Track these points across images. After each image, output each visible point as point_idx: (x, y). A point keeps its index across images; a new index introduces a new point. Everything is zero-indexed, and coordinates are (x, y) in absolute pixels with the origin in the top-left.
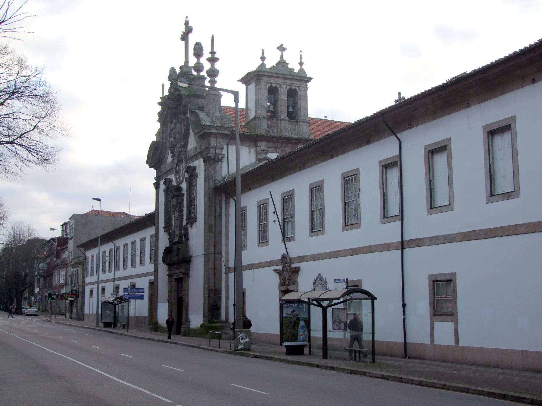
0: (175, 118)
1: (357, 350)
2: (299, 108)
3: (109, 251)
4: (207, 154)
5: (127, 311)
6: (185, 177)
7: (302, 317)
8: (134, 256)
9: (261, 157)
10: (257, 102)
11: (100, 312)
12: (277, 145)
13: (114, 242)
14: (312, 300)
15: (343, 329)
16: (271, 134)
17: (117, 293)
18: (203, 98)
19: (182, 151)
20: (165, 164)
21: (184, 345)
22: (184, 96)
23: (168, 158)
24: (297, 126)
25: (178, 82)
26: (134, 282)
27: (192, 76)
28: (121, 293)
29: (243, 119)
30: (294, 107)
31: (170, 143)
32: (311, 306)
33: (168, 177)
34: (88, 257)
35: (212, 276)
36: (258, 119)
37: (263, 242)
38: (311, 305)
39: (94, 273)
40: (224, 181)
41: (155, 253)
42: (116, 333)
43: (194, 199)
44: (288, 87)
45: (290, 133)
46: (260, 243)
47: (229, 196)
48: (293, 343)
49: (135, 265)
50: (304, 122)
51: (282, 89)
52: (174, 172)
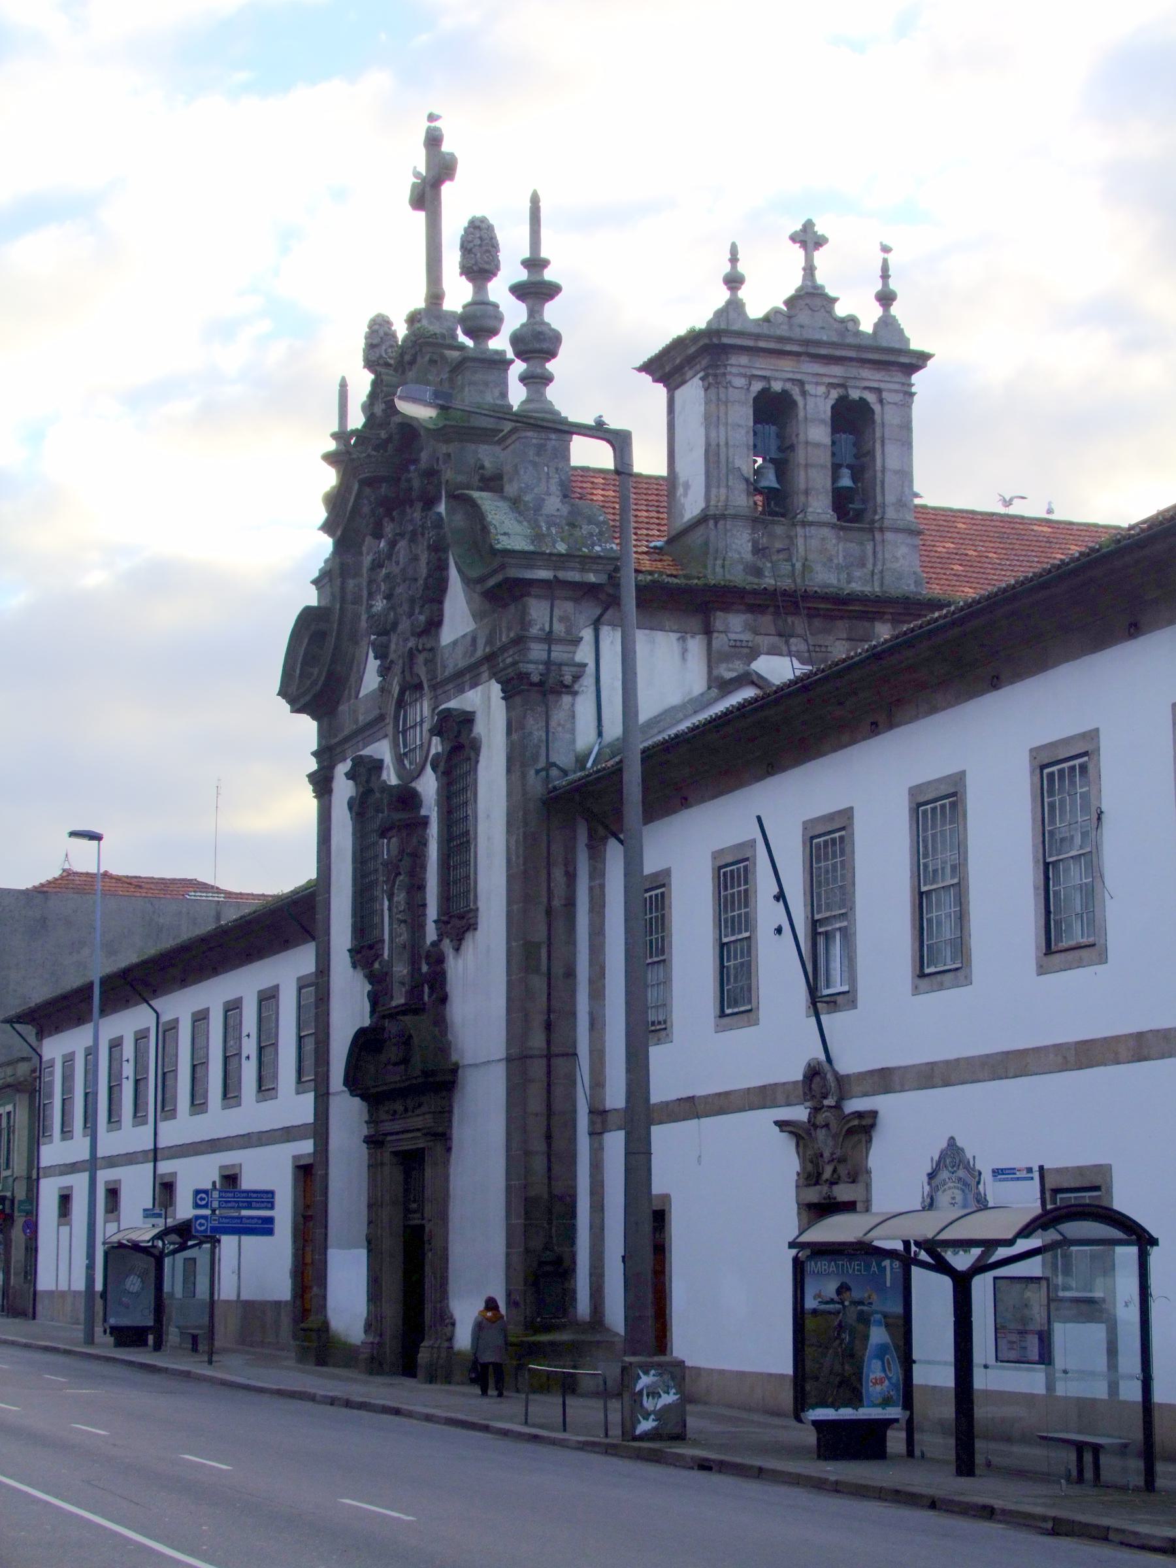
0: (393, 520)
1: (1086, 1443)
2: (879, 475)
3: (136, 1040)
4: (514, 664)
5: (207, 1281)
6: (433, 751)
7: (877, 1312)
8: (233, 1063)
9: (727, 672)
10: (712, 455)
11: (99, 1286)
12: (793, 623)
13: (152, 1003)
14: (917, 1244)
15: (1037, 1358)
16: (768, 581)
17: (170, 1209)
18: (499, 442)
19: (418, 650)
20: (352, 701)
21: (428, 1418)
22: (422, 432)
23: (364, 673)
24: (869, 548)
25: (396, 401)
26: (233, 1166)
27: (455, 354)
28: (184, 1209)
30: (855, 478)
31: (371, 617)
32: (914, 1269)
33: (364, 752)
34: (52, 1061)
35: (539, 1145)
37: (736, 1010)
38: (913, 1267)
39: (76, 1124)
40: (583, 768)
41: (316, 1050)
43: (468, 842)
44: (835, 394)
45: (844, 576)
46: (722, 1015)
47: (601, 831)
48: (846, 1413)
49: (238, 1097)
50: (897, 530)
51: (811, 401)
52: (390, 729)
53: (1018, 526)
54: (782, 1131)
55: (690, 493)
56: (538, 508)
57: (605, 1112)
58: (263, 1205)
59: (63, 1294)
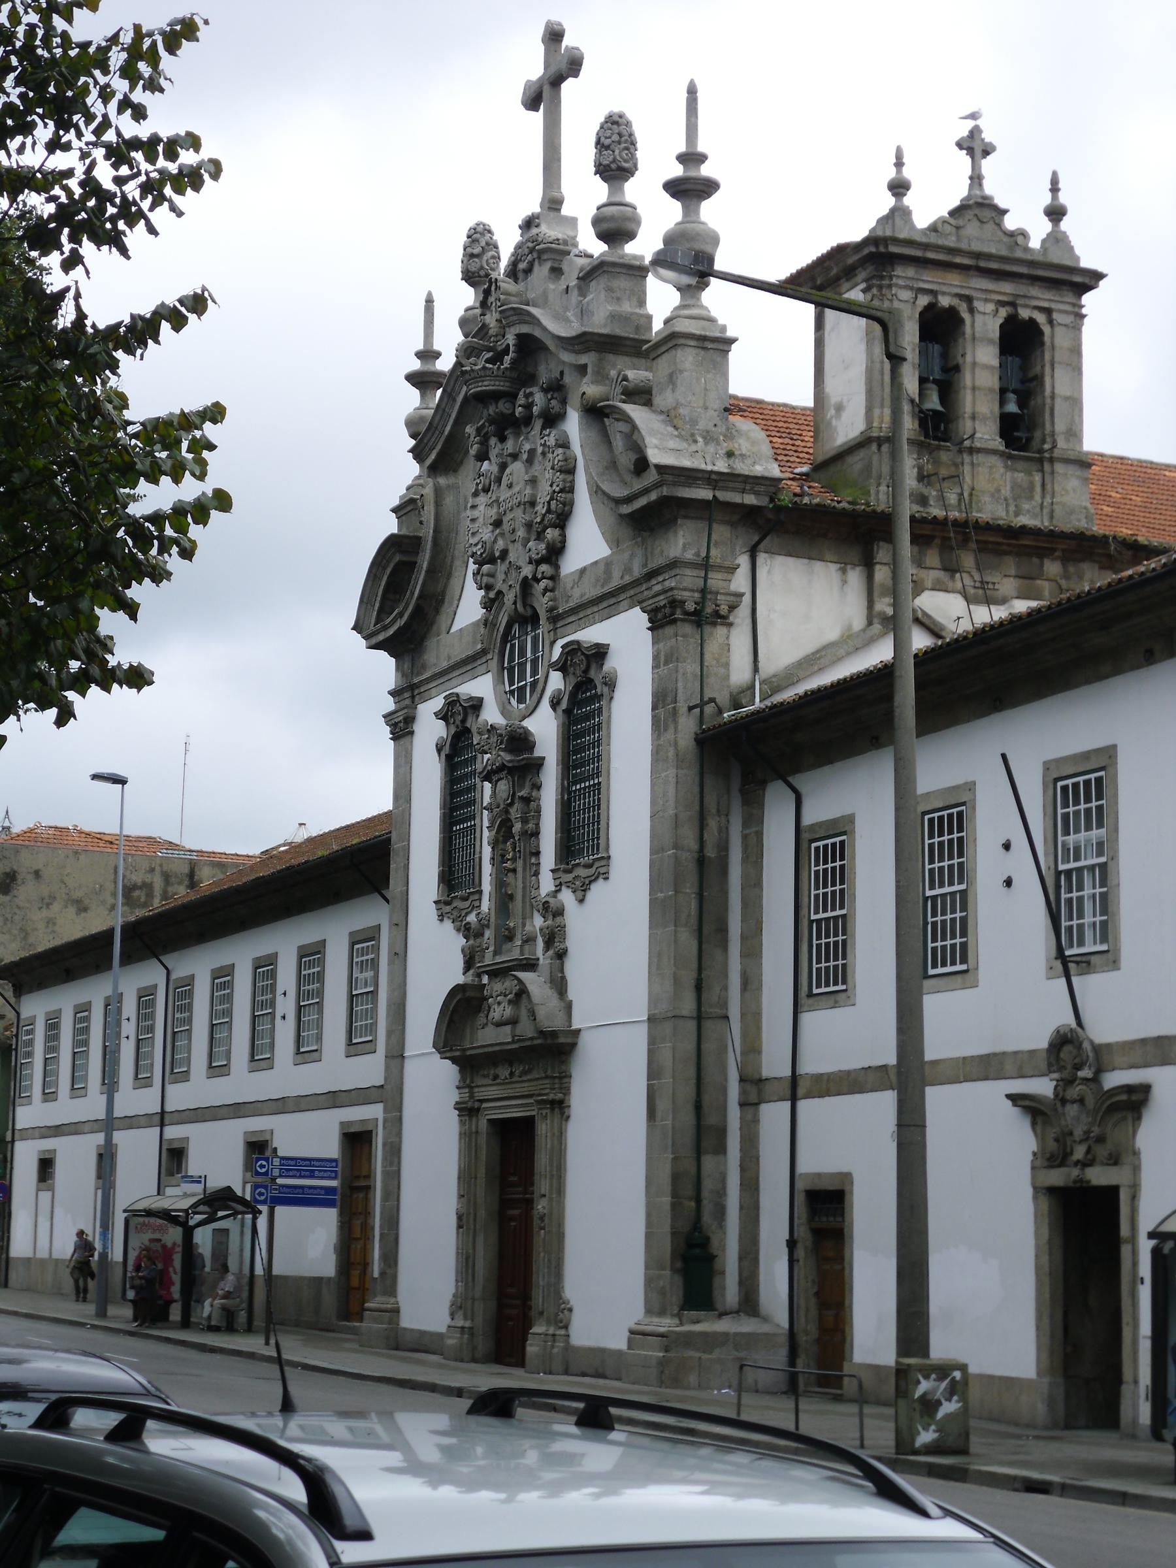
2: (1048, 401)
24: (1037, 478)
29: (793, 445)
30: (1022, 403)
34: (32, 1022)
36: (879, 446)
42: (221, 1351)
44: (1003, 312)
45: (1012, 508)
50: (1067, 461)
51: (979, 319)
52: (494, 664)
53: (1149, 471)
54: (1015, 1105)
55: (845, 415)
56: (694, 422)
57: (760, 1082)
58: (326, 1175)
59: (42, 1262)
